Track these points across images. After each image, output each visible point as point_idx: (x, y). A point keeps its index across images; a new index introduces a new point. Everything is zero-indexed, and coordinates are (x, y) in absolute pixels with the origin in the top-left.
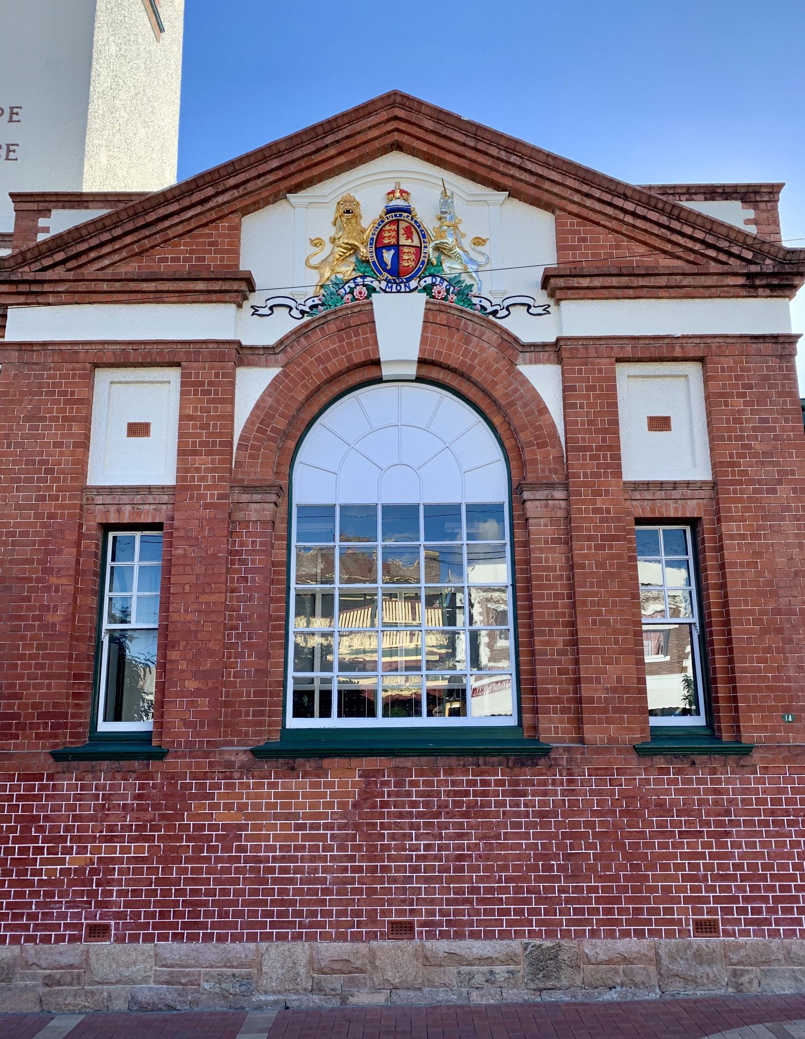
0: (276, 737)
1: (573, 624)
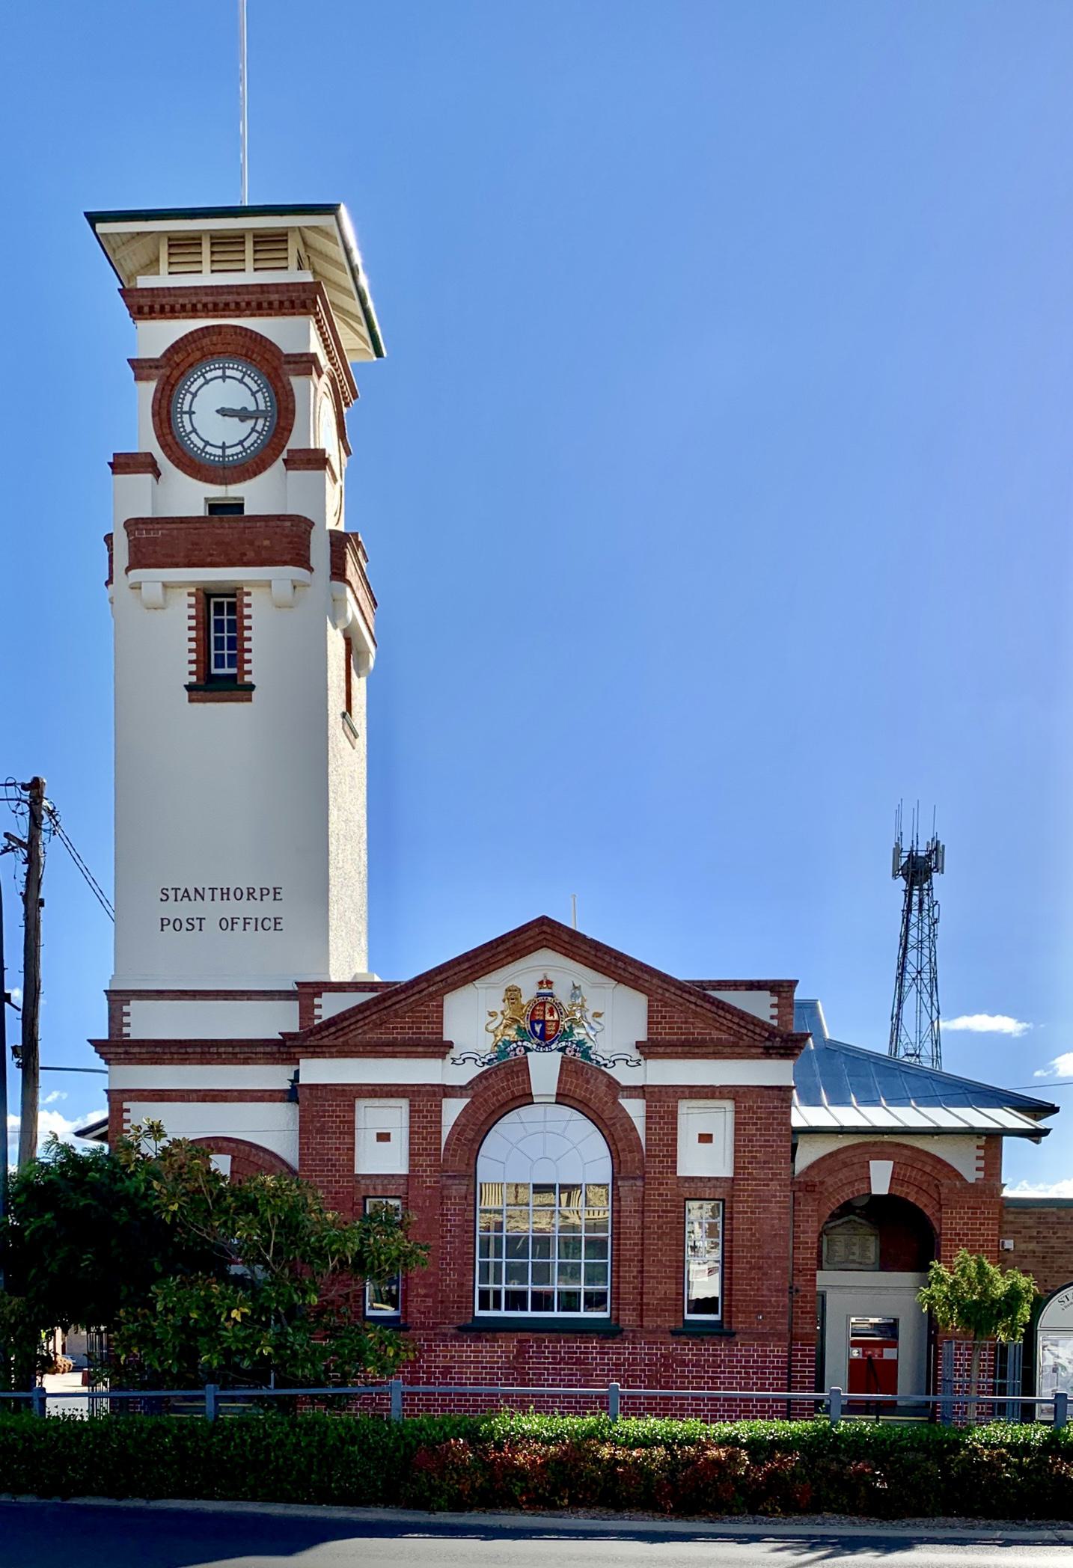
0: (470, 1321)
1: (642, 1261)
